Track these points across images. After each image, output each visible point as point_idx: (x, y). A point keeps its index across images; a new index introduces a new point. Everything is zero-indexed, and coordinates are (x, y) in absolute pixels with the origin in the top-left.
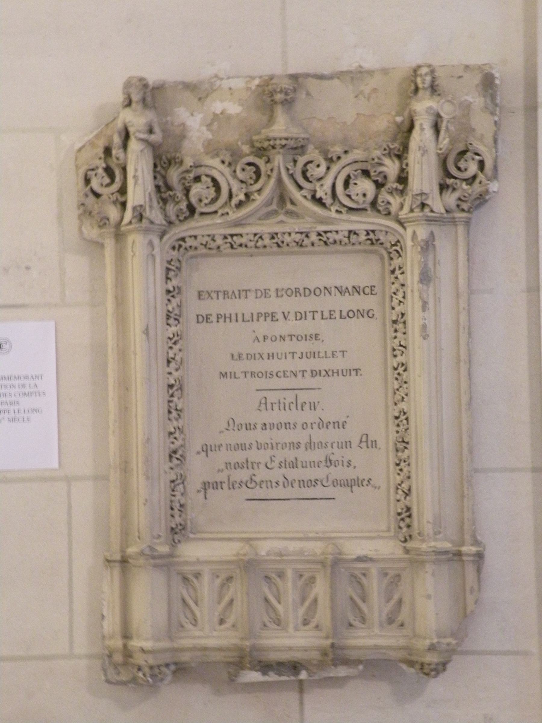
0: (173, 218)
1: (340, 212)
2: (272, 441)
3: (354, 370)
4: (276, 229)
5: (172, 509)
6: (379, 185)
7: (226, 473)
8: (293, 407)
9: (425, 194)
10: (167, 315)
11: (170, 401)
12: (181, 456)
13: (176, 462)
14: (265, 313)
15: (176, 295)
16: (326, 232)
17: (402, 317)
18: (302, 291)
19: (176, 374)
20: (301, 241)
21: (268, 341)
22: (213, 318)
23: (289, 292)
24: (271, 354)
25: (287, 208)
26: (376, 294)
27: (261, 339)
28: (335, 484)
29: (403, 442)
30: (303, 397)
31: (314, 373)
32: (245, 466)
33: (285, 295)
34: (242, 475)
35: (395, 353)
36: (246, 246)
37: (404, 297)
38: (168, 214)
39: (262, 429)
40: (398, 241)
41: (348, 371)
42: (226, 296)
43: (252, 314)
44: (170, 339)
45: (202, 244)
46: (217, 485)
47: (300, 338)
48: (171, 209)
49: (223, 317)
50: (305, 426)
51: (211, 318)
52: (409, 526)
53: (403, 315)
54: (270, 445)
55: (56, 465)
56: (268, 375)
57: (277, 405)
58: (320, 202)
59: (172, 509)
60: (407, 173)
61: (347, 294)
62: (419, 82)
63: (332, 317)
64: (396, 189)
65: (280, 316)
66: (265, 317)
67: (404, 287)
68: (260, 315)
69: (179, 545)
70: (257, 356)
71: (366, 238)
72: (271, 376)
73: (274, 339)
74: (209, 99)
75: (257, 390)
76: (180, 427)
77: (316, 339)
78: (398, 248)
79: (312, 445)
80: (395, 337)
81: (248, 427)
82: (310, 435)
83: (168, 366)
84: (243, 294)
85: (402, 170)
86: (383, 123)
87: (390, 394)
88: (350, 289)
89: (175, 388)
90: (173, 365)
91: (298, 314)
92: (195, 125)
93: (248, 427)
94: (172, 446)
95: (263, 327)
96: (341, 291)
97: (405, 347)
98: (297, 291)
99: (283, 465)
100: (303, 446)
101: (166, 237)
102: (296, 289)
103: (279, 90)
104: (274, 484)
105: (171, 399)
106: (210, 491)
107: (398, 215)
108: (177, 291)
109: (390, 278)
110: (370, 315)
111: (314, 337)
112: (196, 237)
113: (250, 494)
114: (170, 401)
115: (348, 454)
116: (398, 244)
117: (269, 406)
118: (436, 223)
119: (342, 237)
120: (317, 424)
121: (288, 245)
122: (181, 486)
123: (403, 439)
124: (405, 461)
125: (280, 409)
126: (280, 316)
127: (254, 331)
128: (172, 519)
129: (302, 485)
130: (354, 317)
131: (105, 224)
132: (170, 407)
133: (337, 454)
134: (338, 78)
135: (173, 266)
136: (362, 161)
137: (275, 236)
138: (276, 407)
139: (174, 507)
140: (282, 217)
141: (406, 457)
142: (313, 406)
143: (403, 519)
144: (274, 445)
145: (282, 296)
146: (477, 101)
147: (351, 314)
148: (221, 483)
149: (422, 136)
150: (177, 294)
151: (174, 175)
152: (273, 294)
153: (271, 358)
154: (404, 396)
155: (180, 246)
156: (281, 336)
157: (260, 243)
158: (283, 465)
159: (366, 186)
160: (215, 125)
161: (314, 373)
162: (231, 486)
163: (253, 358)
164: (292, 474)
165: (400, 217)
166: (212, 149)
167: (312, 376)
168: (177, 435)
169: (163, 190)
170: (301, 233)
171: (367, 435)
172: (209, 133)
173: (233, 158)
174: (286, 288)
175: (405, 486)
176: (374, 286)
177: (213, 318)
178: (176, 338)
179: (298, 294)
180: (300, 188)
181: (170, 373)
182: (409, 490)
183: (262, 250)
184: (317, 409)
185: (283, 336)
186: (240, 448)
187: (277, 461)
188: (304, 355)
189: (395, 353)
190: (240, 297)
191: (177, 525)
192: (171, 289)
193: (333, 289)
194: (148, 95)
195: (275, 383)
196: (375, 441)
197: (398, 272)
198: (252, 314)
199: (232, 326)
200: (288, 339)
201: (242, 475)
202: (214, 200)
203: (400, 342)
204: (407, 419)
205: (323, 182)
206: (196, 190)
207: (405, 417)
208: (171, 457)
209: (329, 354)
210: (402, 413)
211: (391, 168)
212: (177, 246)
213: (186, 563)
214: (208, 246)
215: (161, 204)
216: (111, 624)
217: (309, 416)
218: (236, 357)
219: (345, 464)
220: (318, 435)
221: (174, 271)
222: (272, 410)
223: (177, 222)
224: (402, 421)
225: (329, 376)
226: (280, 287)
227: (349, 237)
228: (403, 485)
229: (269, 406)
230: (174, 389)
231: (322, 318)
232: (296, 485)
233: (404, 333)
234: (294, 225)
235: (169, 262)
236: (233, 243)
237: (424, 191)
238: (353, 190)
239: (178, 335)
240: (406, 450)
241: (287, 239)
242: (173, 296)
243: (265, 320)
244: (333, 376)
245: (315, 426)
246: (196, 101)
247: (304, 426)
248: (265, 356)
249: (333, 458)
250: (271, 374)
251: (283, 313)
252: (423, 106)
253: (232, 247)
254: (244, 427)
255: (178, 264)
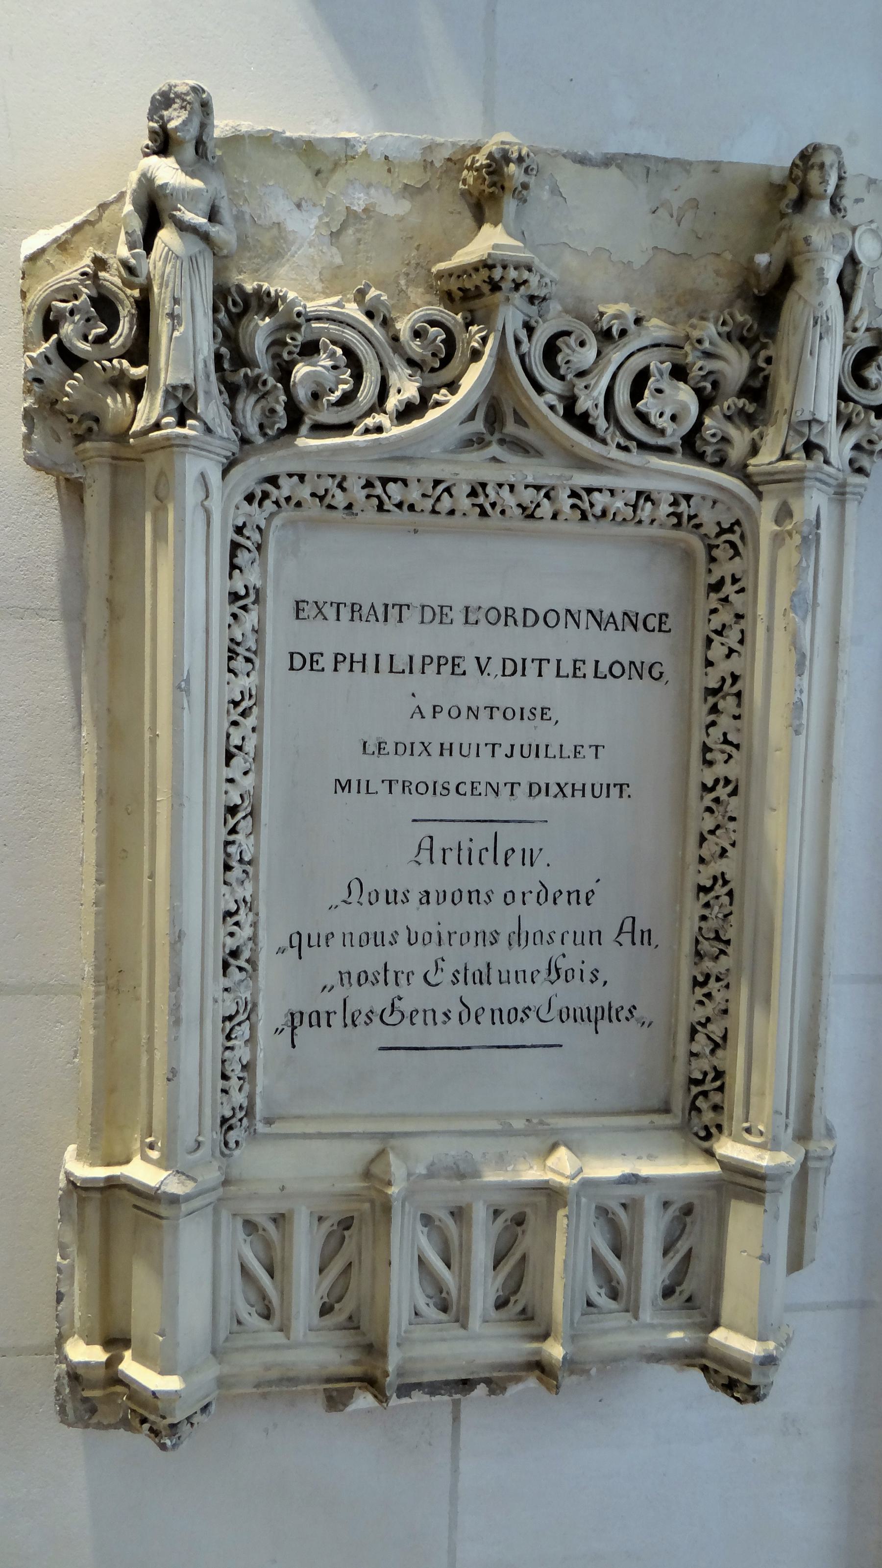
0: (253, 429)
1: (626, 449)
2: (440, 928)
3: (615, 785)
4: (490, 474)
5: (225, 1077)
6: (705, 403)
7: (339, 993)
8: (488, 857)
9: (819, 422)
10: (230, 650)
11: (227, 843)
12: (248, 961)
13: (236, 975)
14: (439, 658)
15: (251, 606)
16: (589, 491)
17: (733, 684)
18: (519, 616)
19: (247, 783)
20: (534, 506)
21: (443, 716)
22: (327, 662)
23: (493, 615)
24: (447, 746)
25: (505, 431)
26: (670, 631)
27: (428, 711)
28: (564, 1017)
29: (718, 938)
30: (509, 837)
31: (535, 790)
32: (381, 978)
33: (483, 621)
34: (375, 998)
35: (709, 756)
36: (411, 508)
37: (741, 642)
38: (240, 419)
39: (421, 903)
40: (738, 523)
41: (605, 787)
42: (356, 615)
43: (411, 658)
44: (236, 704)
45: (313, 495)
46: (317, 1019)
47: (509, 714)
48: (250, 411)
49: (348, 660)
50: (509, 899)
51: (321, 660)
52: (717, 1108)
53: (735, 678)
54: (435, 938)
56: (439, 789)
57: (456, 852)
58: (583, 423)
59: (225, 1077)
60: (766, 378)
61: (611, 627)
63: (578, 673)
64: (741, 411)
65: (469, 665)
66: (439, 665)
67: (742, 621)
68: (428, 660)
69: (237, 1153)
70: (418, 748)
71: (671, 510)
72: (445, 792)
73: (454, 713)
74: (338, 177)
75: (414, 821)
76: (248, 899)
77: (542, 718)
78: (735, 538)
79: (523, 937)
80: (713, 724)
81: (391, 898)
83: (227, 764)
84: (393, 613)
85: (755, 371)
87: (693, 839)
88: (619, 618)
89: (241, 815)
90: (238, 762)
91: (508, 662)
93: (391, 898)
94: (229, 940)
95: (433, 687)
96: (599, 620)
97: (737, 747)
98: (508, 615)
99: (461, 977)
100: (503, 939)
101: (236, 472)
102: (506, 609)
103: (515, 155)
104: (440, 1018)
105: (231, 838)
106: (303, 1031)
107: (746, 466)
108: (252, 597)
109: (705, 602)
110: (656, 674)
111: (538, 713)
112: (302, 477)
113: (388, 1036)
114: (227, 843)
115: (592, 956)
116: (736, 528)
117: (438, 855)
118: (824, 487)
119: (619, 504)
120: (535, 895)
121: (503, 512)
122: (246, 1026)
123: (717, 932)
124: (718, 979)
125: (459, 863)
126: (469, 665)
127: (413, 695)
128: (225, 1097)
129: (348, 942)
130: (622, 675)
131: (90, 430)
132: (228, 855)
133: (574, 957)
134: (620, 167)
135: (248, 538)
136: (667, 346)
137: (480, 490)
138: (451, 857)
139: (229, 1073)
140: (495, 450)
141: (723, 971)
142: (529, 858)
143: (705, 1094)
144: (445, 937)
147: (617, 670)
148: (328, 1013)
150: (253, 603)
152: (460, 617)
153: (446, 753)
154: (728, 847)
155: (265, 495)
156: (470, 708)
157: (446, 503)
158: (461, 977)
160: (350, 235)
161: (535, 789)
162: (349, 1021)
163: (409, 751)
164: (479, 996)
165: (750, 469)
167: (531, 795)
168: (241, 917)
169: (231, 358)
170: (538, 488)
171: (634, 918)
172: (334, 250)
174: (485, 607)
175: (716, 1030)
176: (667, 616)
177: (327, 662)
178: (245, 704)
179: (510, 621)
180: (540, 389)
181: (231, 781)
182: (725, 1038)
183: (442, 520)
184: (535, 865)
185: (475, 709)
186: (372, 941)
187: (448, 968)
188: (517, 750)
189: (709, 756)
190: (386, 620)
191: (233, 1109)
192: (242, 592)
193: (584, 614)
195: (451, 806)
196: (649, 931)
197: (729, 589)
198: (411, 658)
199: (365, 680)
200: (484, 714)
201: (375, 998)
202: (347, 398)
203: (725, 734)
204: (730, 894)
205: (589, 380)
207: (726, 889)
208: (226, 966)
209: (568, 751)
210: (720, 882)
212: (259, 495)
213: (253, 1196)
214: (328, 500)
215: (226, 395)
217: (519, 878)
218: (372, 747)
219: (587, 976)
220: (536, 917)
221: (249, 551)
222: (444, 863)
223: (260, 440)
224: (717, 897)
225: (564, 796)
226: (474, 605)
227: (635, 507)
228: (711, 1027)
229: (438, 855)
231: (558, 675)
232: (485, 1018)
233: (737, 717)
234: (529, 471)
235: (239, 530)
236: (385, 498)
237: (818, 417)
238: (648, 403)
239: (251, 696)
240: (722, 957)
241: (508, 499)
242: (244, 608)
243: (439, 673)
244: (573, 795)
245: (531, 899)
246: (308, 176)
247: (509, 897)
248: (435, 749)
249: (563, 965)
250: (444, 788)
251: (478, 659)
253: (381, 508)
254: (382, 897)
255: (256, 537)
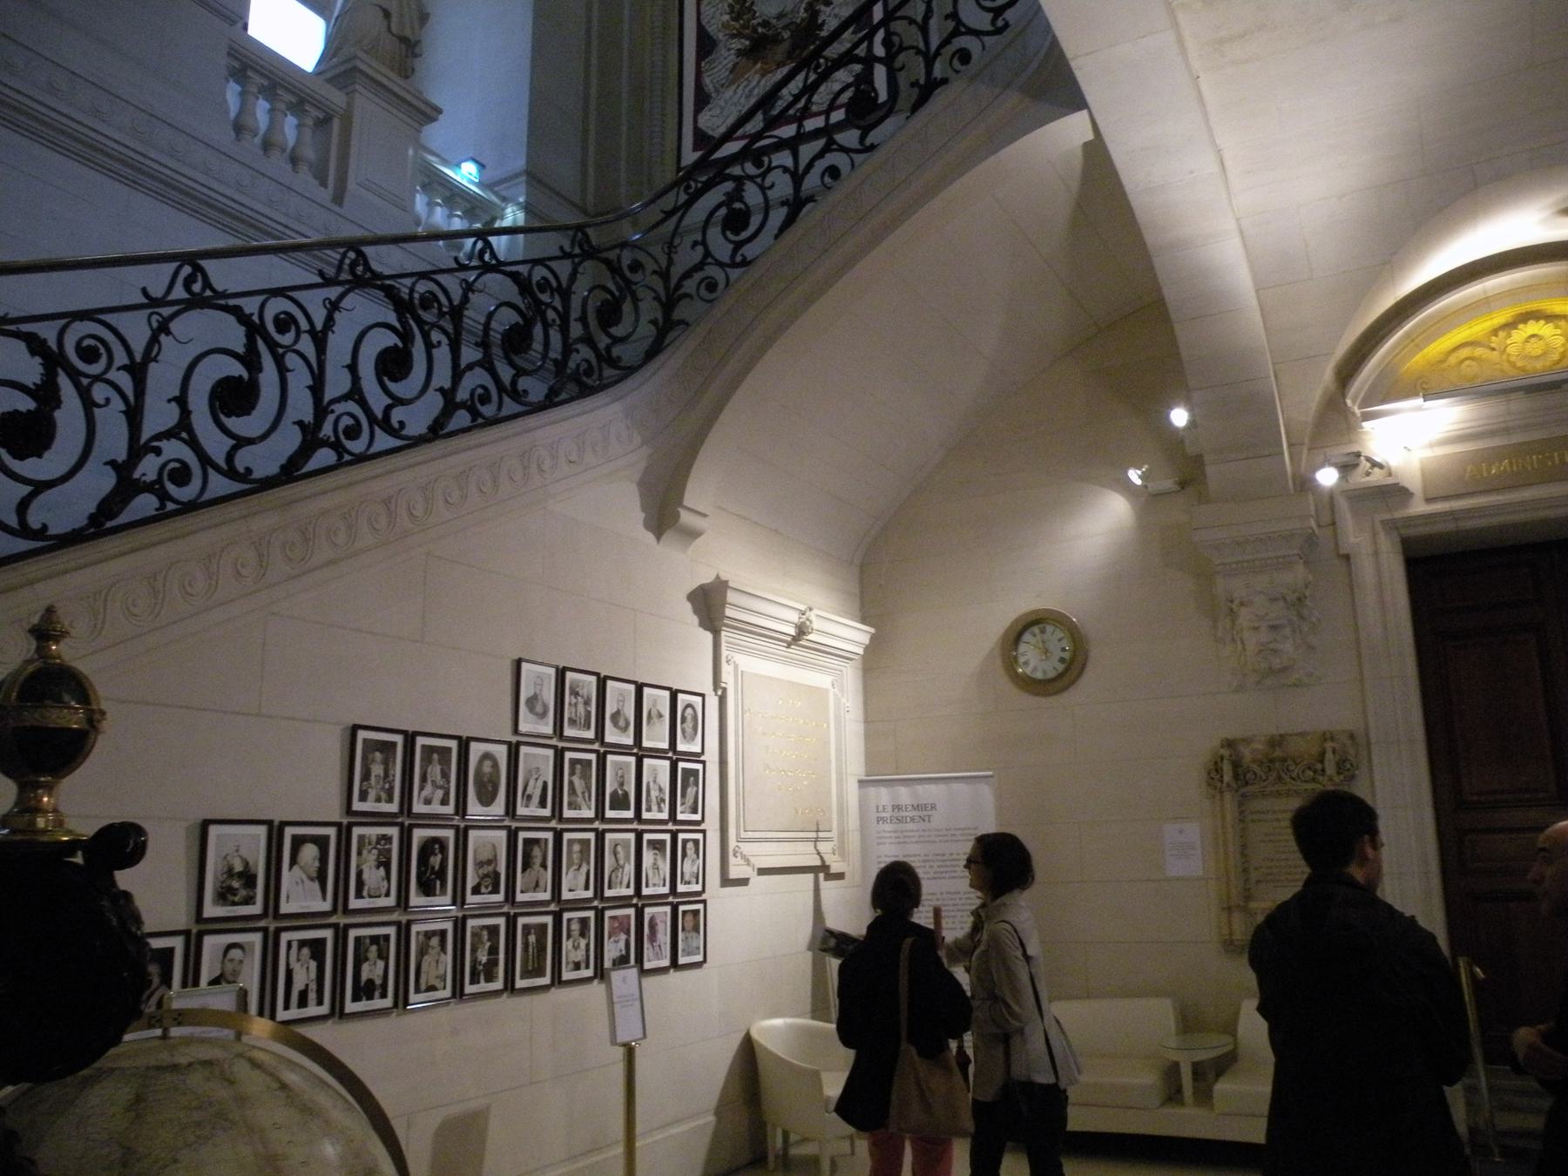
55: (1073, 1125)
62: (1327, 737)
82: (776, 237)
86: (1315, 751)
92: (1247, 753)
145: (108, 400)
146: (1349, 742)
149: (1329, 755)
151: (1240, 771)
159: (1310, 773)
166: (1254, 761)
169: (1236, 776)
173: (1261, 763)
194: (1230, 744)
206: (1249, 776)
211: (1319, 766)
216: (1225, 931)
230: (1244, 846)
252: (1329, 745)
